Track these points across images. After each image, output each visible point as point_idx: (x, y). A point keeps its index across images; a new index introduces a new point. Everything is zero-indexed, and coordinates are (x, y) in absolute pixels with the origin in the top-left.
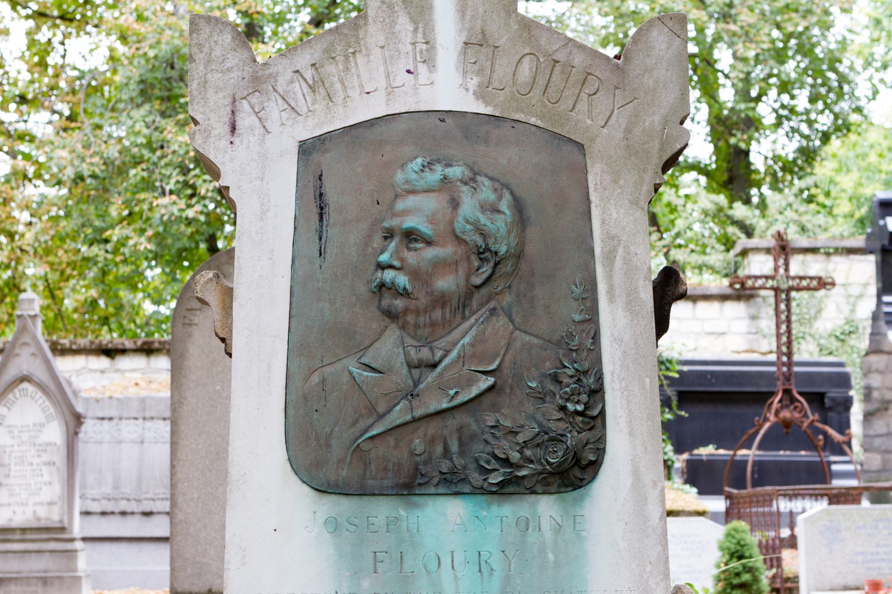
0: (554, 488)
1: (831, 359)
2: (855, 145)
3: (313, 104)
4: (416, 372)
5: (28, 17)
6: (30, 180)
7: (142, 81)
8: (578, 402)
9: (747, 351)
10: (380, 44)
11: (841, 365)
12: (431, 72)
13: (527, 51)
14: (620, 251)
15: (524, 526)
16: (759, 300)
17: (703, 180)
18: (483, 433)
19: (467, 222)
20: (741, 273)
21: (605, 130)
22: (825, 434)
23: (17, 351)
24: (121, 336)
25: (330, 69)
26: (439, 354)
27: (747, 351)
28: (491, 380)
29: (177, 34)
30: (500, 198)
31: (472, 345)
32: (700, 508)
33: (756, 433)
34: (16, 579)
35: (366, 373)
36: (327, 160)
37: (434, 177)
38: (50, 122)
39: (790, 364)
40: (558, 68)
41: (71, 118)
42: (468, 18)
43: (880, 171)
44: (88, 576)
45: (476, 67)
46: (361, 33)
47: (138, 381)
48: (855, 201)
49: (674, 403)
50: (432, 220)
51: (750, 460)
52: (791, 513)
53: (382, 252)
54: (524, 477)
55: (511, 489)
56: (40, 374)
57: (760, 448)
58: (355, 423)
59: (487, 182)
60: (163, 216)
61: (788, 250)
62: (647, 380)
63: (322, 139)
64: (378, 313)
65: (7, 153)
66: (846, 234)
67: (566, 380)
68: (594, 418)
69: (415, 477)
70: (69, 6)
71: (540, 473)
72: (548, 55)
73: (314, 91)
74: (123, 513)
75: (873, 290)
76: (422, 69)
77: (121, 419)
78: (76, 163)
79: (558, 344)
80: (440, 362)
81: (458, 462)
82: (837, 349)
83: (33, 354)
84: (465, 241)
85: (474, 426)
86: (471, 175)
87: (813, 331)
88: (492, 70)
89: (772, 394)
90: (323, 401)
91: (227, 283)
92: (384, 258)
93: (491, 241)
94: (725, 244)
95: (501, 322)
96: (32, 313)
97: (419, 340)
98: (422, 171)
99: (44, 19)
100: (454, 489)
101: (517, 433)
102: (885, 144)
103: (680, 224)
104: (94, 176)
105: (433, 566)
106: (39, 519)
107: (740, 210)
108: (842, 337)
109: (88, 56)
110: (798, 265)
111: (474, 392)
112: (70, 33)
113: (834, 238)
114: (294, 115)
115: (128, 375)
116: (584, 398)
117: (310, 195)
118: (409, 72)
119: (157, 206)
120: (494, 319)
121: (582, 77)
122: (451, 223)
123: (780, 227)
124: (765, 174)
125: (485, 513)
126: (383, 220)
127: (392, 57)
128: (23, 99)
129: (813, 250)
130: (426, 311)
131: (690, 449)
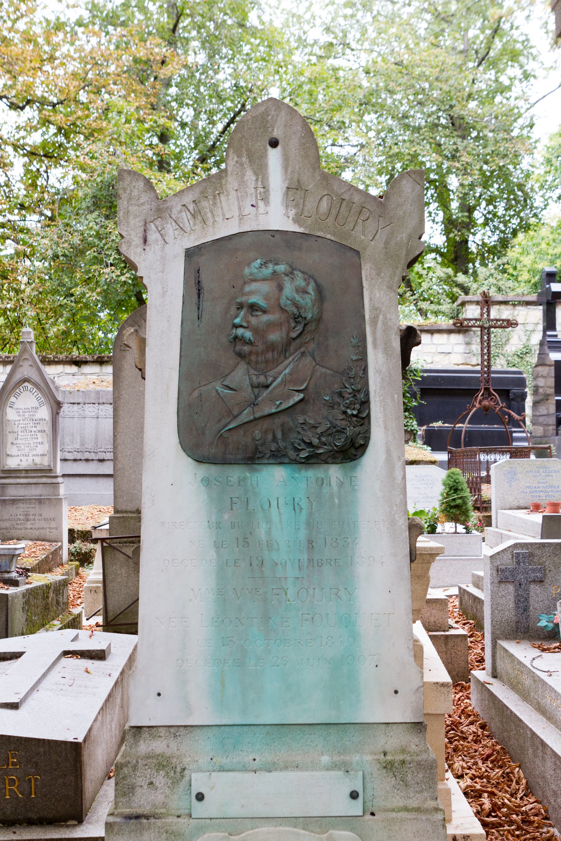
0: (339, 460)
1: (514, 369)
2: (532, 238)
3: (194, 226)
4: (256, 391)
5: (24, 155)
6: (28, 257)
7: (95, 197)
8: (354, 409)
9: (463, 364)
10: (235, 188)
11: (520, 373)
12: (266, 206)
13: (326, 193)
14: (381, 317)
15: (321, 482)
16: (472, 333)
17: (439, 259)
18: (296, 427)
19: (288, 299)
20: (461, 317)
21: (373, 243)
22: (509, 415)
23: (21, 363)
24: (84, 352)
26: (270, 379)
27: (463, 364)
28: (302, 396)
29: (115, 168)
30: (308, 284)
31: (290, 374)
32: (433, 459)
33: (468, 414)
34: (23, 500)
35: (226, 391)
36: (203, 261)
37: (268, 271)
38: (39, 221)
39: (489, 372)
40: (344, 204)
41: (52, 219)
42: (289, 172)
43: (548, 254)
44: (66, 498)
45: (294, 203)
46: (223, 181)
47: (95, 381)
48: (532, 273)
49: (419, 396)
50: (266, 298)
51: (464, 430)
52: (487, 461)
53: (236, 317)
54: (321, 454)
55: (313, 461)
56: (35, 377)
57: (469, 423)
58: (219, 421)
59: (300, 275)
60: (107, 279)
61: (489, 303)
62: (396, 396)
64: (233, 354)
65: (13, 240)
66: (525, 292)
67: (347, 396)
68: (363, 418)
69: (255, 453)
70: (50, 148)
71: (331, 451)
72: (338, 195)
73: (194, 218)
74: (87, 460)
75: (541, 327)
76: (261, 204)
77: (85, 404)
78: (54, 247)
79: (342, 373)
80: (271, 384)
81: (282, 444)
82: (518, 363)
83: (30, 365)
84: (286, 311)
85: (291, 423)
86: (290, 270)
87: (503, 352)
88: (304, 205)
89: (478, 390)
90: (200, 408)
91: (143, 335)
92: (237, 321)
93: (302, 311)
94: (451, 298)
95: (308, 360)
96: (30, 340)
97: (258, 371)
98: (260, 267)
99: (34, 157)
100: (279, 460)
101: (317, 427)
102: (551, 237)
103: (425, 285)
104: (64, 255)
105: (266, 506)
106: (36, 464)
107: (461, 278)
108: (522, 355)
109: (62, 180)
110: (495, 312)
111: (291, 402)
112: (51, 165)
113: (518, 295)
114: (182, 232)
115: (89, 377)
116: (357, 406)
117: (192, 282)
118: (253, 206)
119: (103, 273)
120: (304, 358)
121: (359, 209)
122: (278, 299)
123: (485, 288)
124: (477, 254)
125: (297, 475)
126: (237, 298)
127: (242, 196)
128: (22, 207)
129: (505, 303)
130: (262, 353)
131: (427, 423)
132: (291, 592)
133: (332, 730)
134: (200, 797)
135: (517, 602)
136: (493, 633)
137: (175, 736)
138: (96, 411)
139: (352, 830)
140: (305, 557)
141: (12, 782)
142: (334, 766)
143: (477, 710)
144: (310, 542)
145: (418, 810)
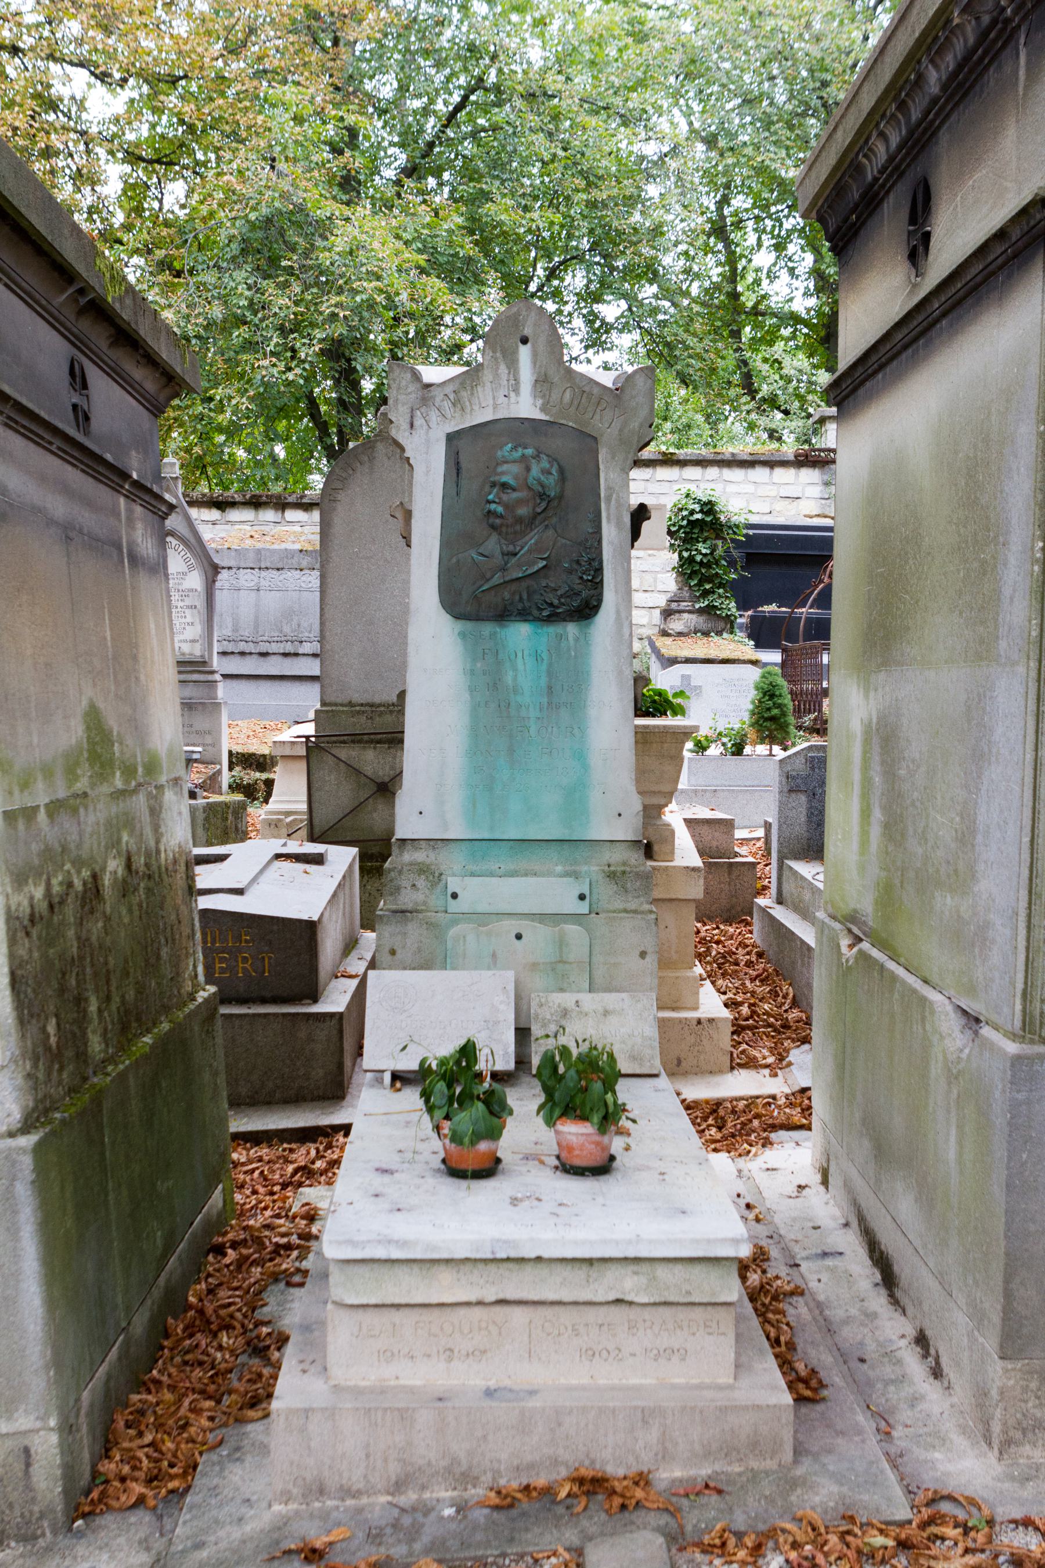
15: (560, 637)
25: (464, 394)
31: (536, 544)
32: (753, 658)
37: (517, 454)
63: (459, 433)
74: (242, 654)
76: (512, 394)
79: (580, 544)
81: (527, 604)
92: (491, 497)
95: (550, 532)
105: (513, 657)
106: (183, 654)
111: (536, 568)
115: (237, 527)
122: (526, 479)
132: (533, 730)
133: (566, 845)
134: (455, 896)
135: (810, 816)
136: (779, 852)
137: (434, 848)
138: (256, 580)
139: (580, 925)
140: (545, 700)
141: (245, 959)
142: (567, 874)
143: (759, 942)
144: (550, 688)
145: (635, 912)
